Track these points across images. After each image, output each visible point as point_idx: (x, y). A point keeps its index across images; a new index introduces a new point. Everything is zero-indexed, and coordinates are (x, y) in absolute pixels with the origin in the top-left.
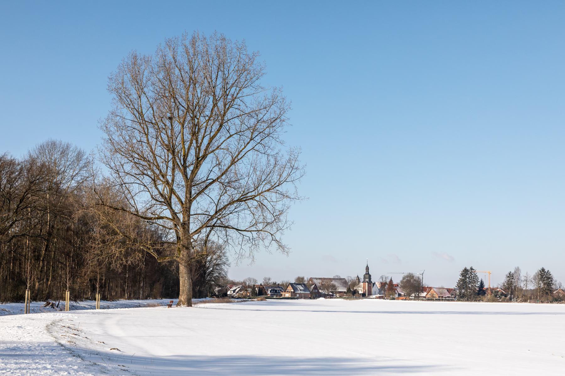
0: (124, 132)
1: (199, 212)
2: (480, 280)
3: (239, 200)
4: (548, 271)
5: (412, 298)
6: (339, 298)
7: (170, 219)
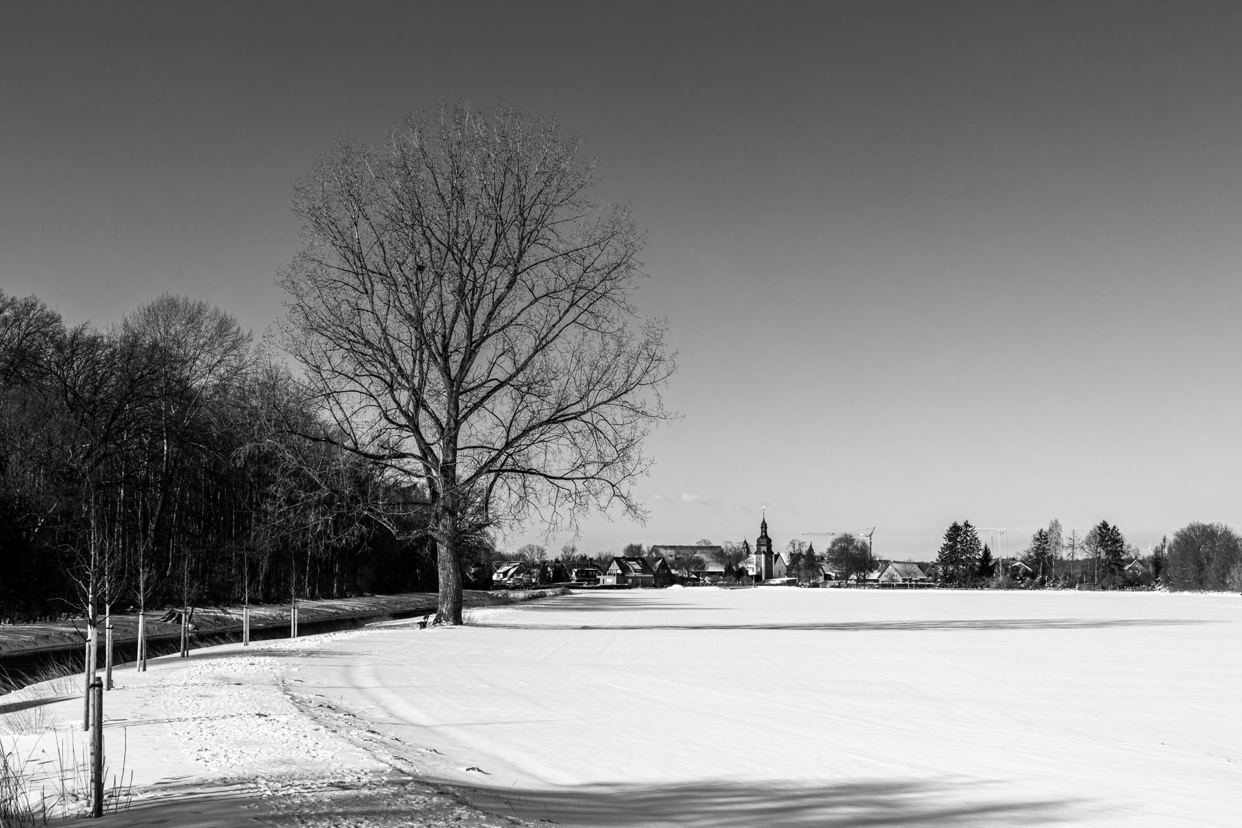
1: (475, 443)
2: (983, 547)
4: (1114, 527)
6: (710, 585)
7: (418, 457)
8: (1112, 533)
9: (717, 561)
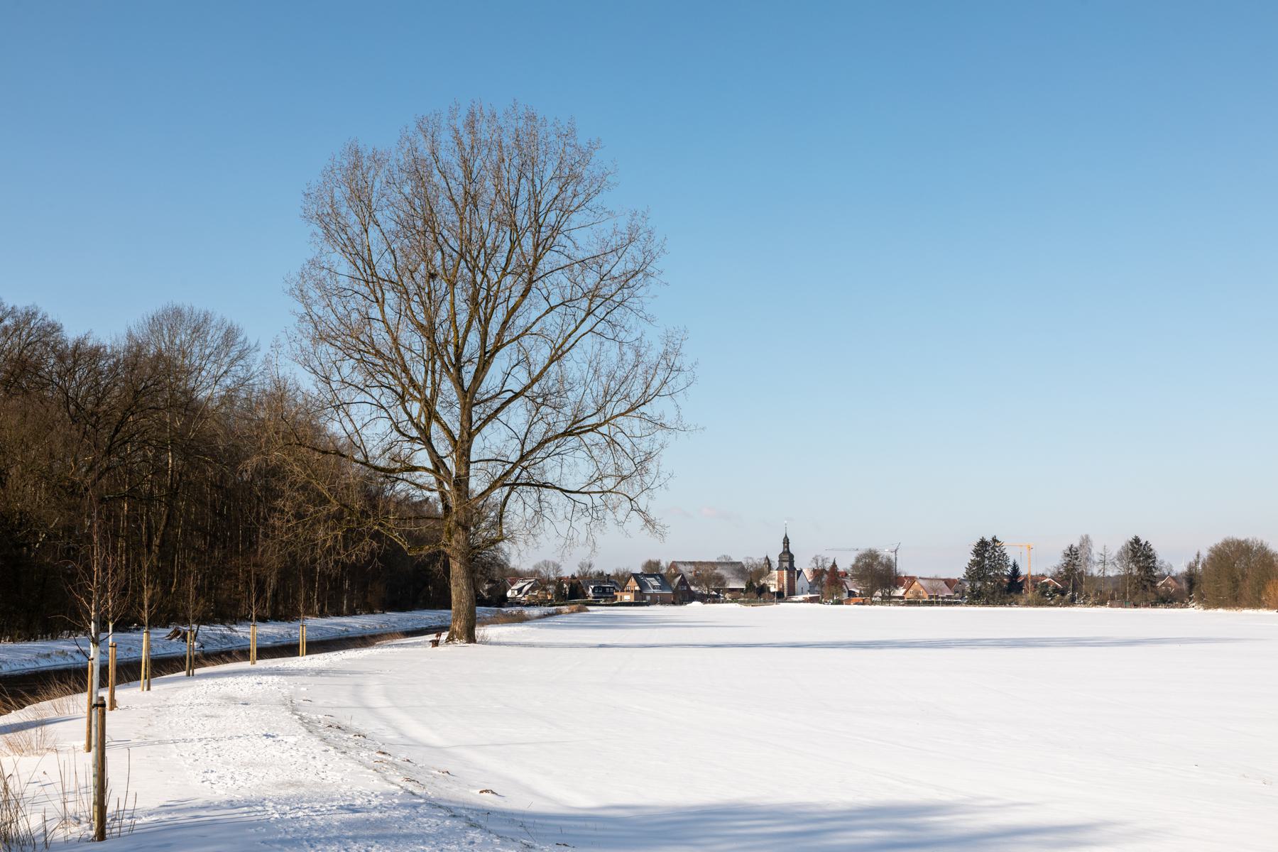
0: (334, 300)
3: (567, 433)
4: (1147, 542)
5: (876, 599)
6: (731, 602)
7: (431, 470)
8: (1144, 549)
9: (737, 577)
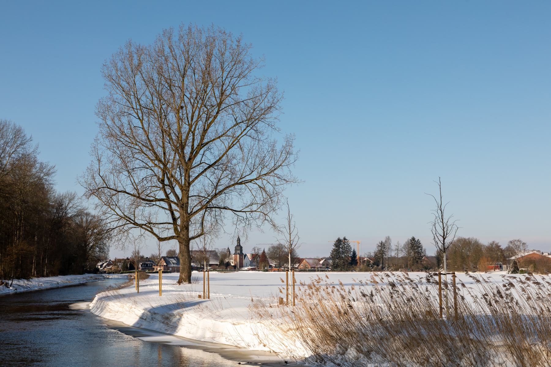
2: (352, 250)
4: (418, 240)
8: (417, 243)
9: (213, 258)
